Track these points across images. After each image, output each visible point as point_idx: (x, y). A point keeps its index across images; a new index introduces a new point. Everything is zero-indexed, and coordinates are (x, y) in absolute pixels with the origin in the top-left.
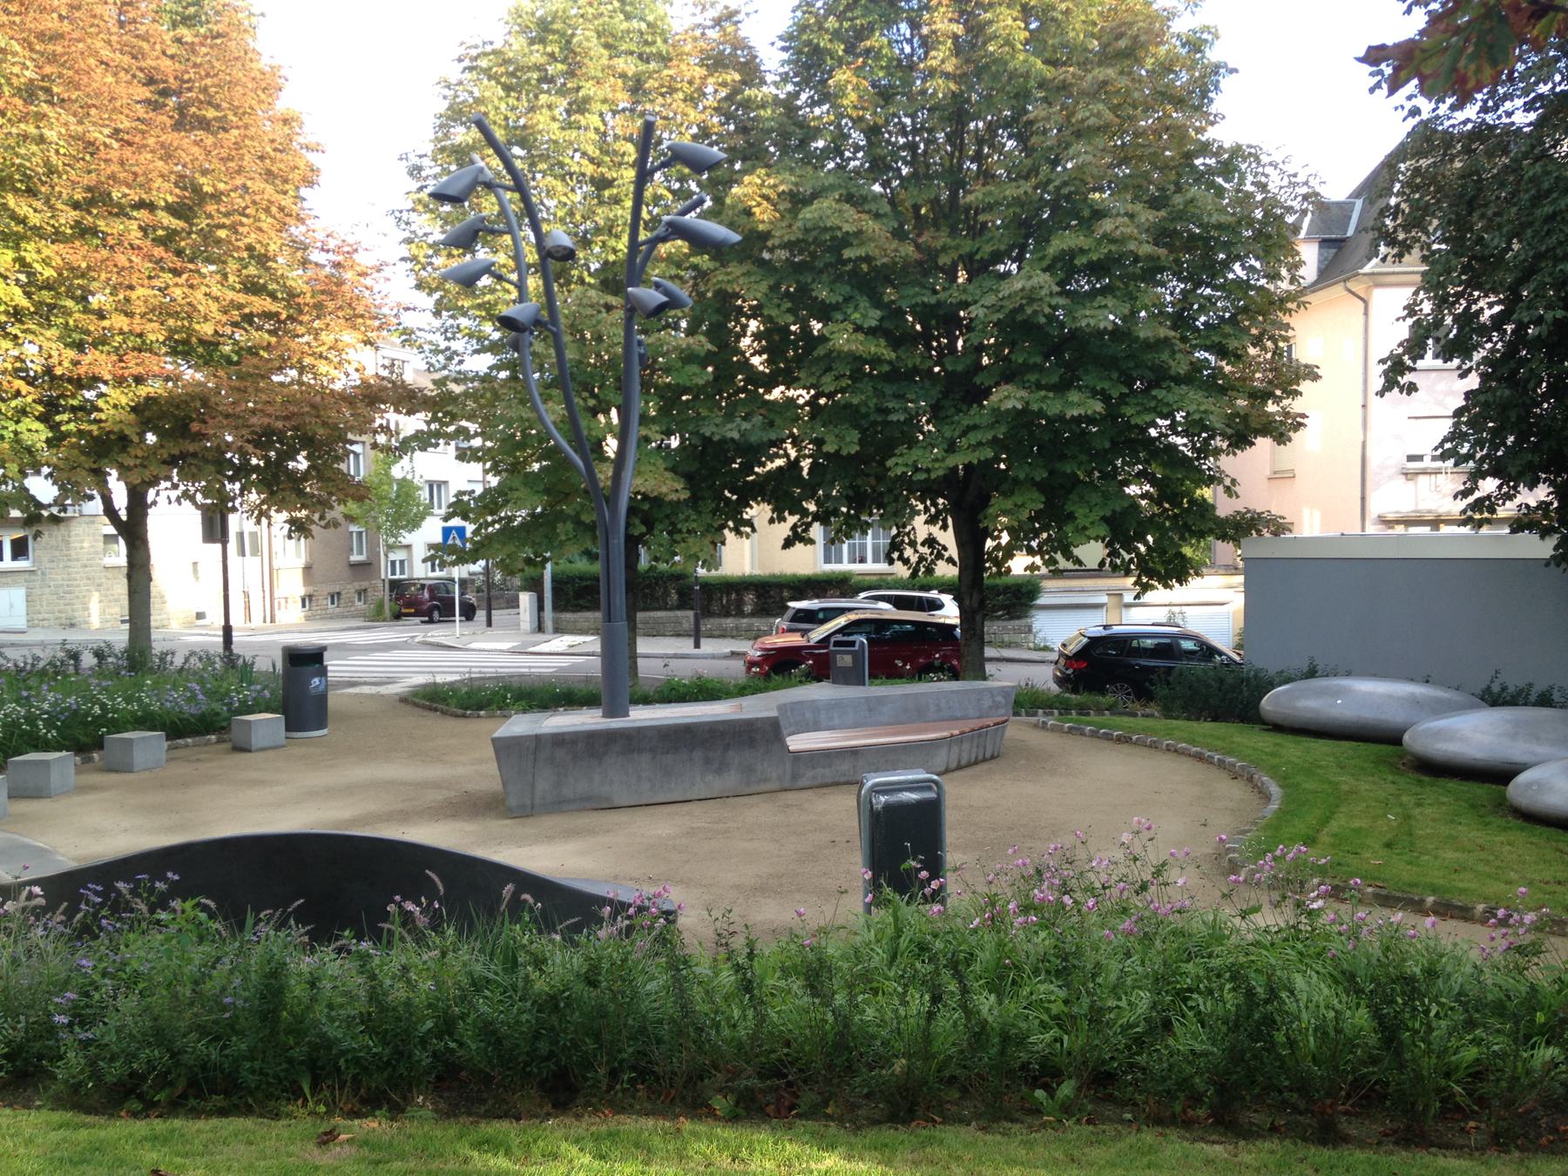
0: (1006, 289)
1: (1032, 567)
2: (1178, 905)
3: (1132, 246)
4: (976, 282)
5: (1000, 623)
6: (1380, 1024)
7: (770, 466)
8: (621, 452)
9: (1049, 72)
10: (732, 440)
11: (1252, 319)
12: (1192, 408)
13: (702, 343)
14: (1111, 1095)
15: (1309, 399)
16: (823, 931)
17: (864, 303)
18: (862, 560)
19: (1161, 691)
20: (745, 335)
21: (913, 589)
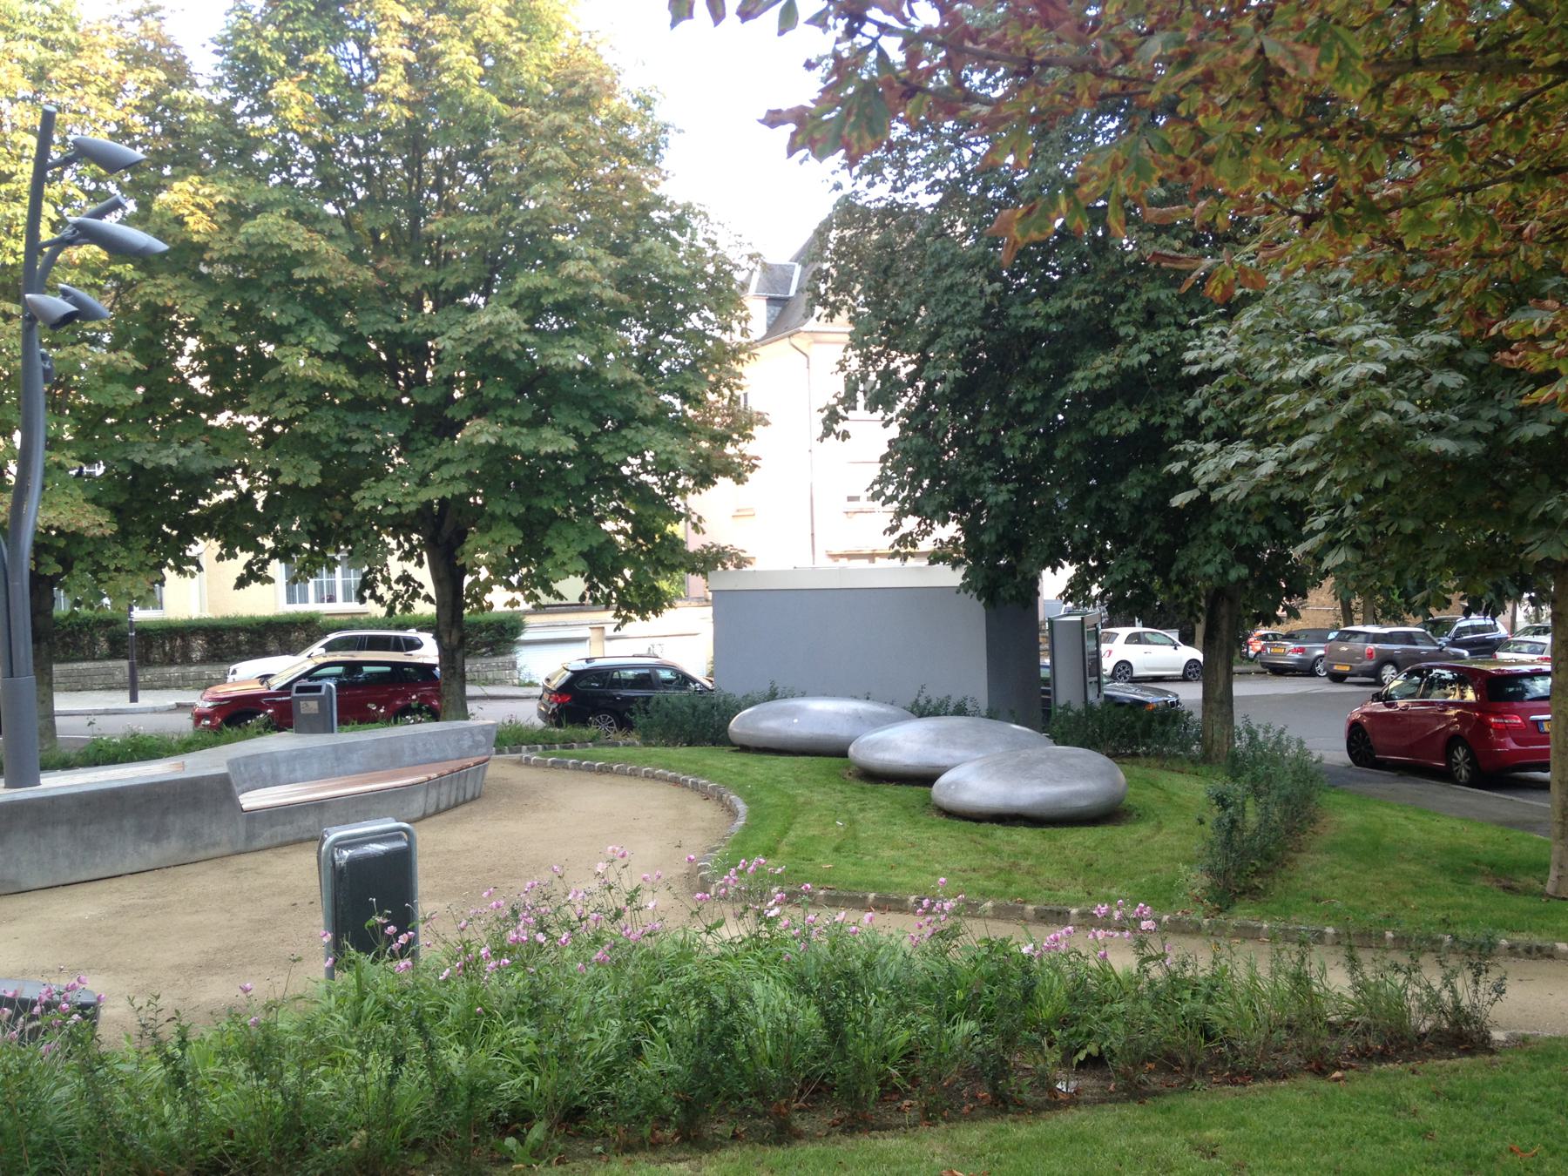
0: (473, 322)
1: (513, 603)
2: (648, 929)
3: (596, 290)
4: (444, 312)
5: (483, 660)
6: (828, 1019)
7: (216, 499)
8: (23, 476)
9: (506, 111)
10: (169, 467)
11: (710, 367)
12: (660, 448)
13: (127, 360)
14: (582, 1130)
15: (759, 445)
16: (269, 1008)
17: (320, 326)
18: (331, 599)
19: (640, 720)
20: (182, 354)
21: (389, 628)
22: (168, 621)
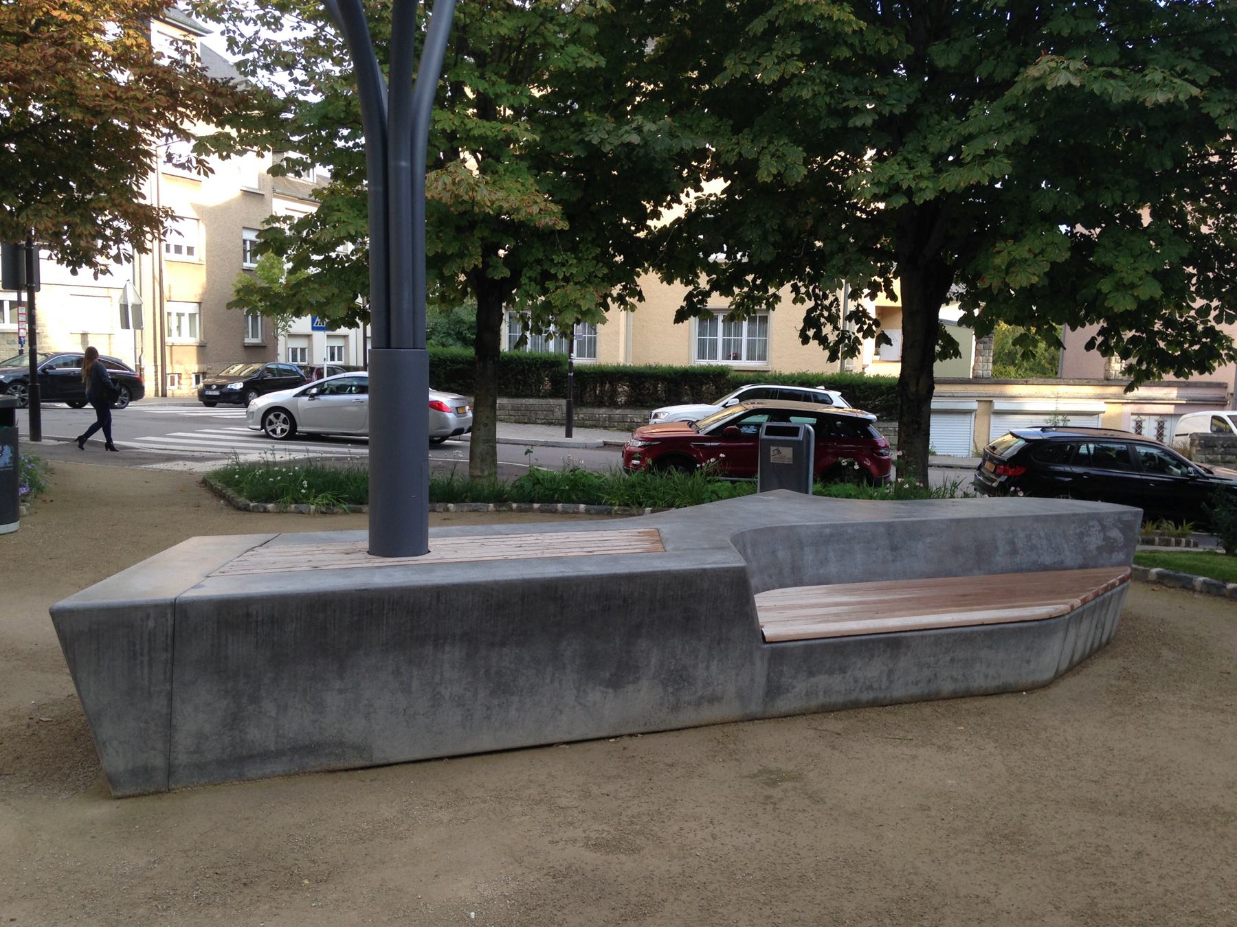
22: (600, 366)
